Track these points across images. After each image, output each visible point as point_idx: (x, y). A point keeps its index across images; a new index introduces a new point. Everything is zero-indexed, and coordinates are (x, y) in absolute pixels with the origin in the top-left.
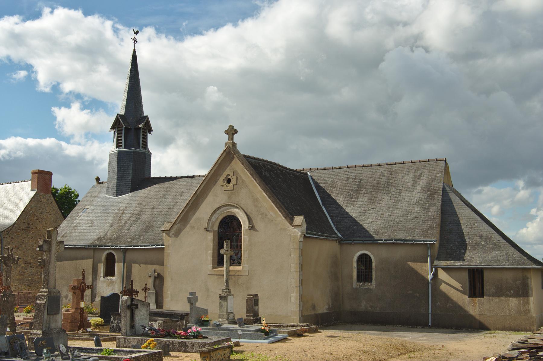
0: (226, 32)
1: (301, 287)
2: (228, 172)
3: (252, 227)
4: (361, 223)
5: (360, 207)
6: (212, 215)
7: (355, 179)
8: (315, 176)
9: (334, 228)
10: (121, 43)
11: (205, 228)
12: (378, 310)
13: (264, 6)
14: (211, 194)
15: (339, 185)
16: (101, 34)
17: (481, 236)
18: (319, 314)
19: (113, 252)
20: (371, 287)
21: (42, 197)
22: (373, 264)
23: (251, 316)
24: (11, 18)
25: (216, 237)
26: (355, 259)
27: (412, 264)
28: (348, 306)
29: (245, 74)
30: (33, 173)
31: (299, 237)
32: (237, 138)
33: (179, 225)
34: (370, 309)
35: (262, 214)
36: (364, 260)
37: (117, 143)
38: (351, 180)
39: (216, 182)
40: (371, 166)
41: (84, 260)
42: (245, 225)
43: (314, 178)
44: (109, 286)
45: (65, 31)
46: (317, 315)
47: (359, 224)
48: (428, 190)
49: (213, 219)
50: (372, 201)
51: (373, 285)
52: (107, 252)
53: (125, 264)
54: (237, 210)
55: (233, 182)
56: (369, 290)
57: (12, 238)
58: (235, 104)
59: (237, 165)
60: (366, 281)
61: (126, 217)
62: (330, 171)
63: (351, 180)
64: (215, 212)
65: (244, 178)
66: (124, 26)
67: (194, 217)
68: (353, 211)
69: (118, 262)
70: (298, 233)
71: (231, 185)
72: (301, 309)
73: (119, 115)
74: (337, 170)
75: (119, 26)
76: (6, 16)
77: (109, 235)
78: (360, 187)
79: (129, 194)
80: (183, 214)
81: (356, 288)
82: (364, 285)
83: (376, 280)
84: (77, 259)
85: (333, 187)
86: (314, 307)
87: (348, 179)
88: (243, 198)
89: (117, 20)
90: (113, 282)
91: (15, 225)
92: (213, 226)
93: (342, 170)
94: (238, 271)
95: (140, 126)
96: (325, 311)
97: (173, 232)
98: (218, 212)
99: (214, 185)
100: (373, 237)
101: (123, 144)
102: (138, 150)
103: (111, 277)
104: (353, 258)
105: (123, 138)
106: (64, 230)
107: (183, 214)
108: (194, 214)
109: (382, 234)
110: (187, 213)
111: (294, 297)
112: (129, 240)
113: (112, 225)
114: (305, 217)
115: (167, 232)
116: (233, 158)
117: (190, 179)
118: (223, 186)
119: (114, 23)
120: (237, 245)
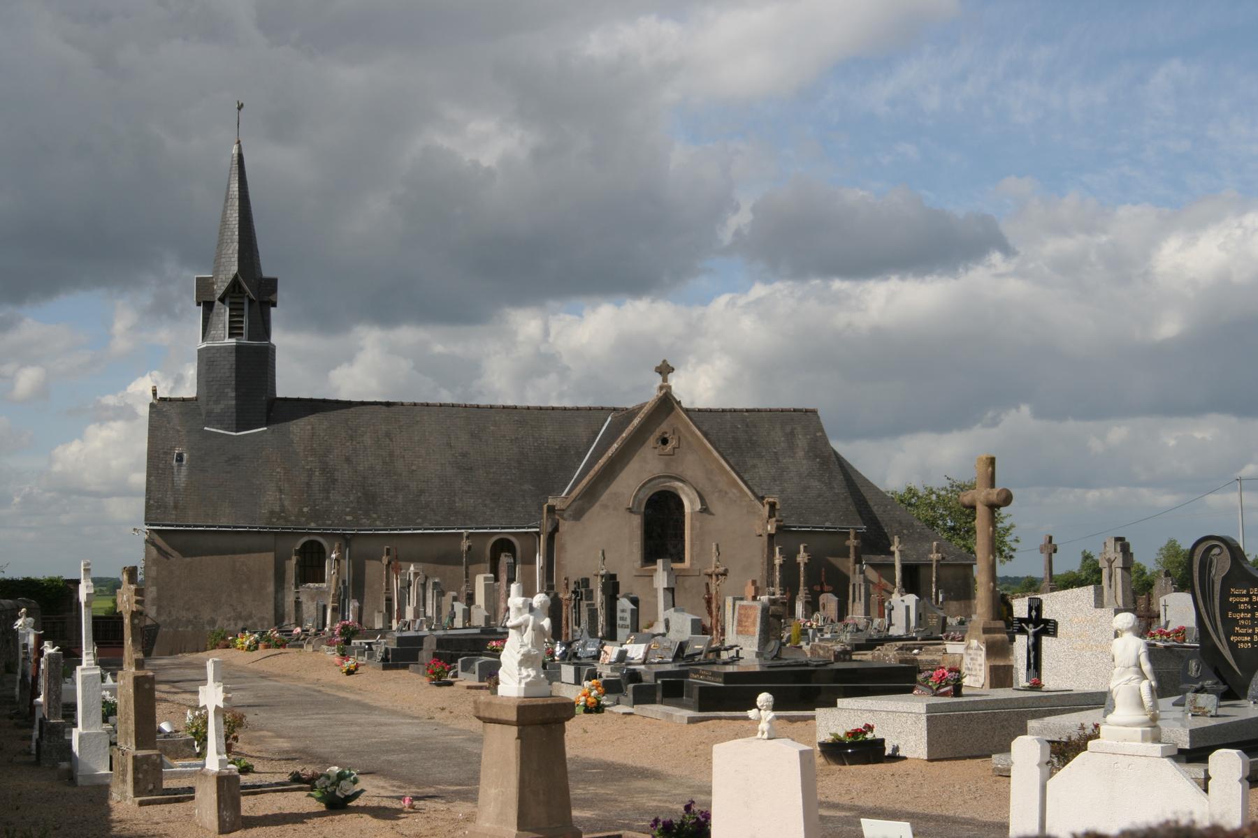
2: (664, 427)
17: (900, 523)
19: (513, 539)
27: (833, 560)
39: (644, 442)
42: (690, 505)
48: (816, 456)
52: (305, 539)
54: (680, 484)
55: (672, 443)
67: (608, 491)
71: (669, 447)
88: (690, 465)
108: (607, 486)
117: (384, 408)
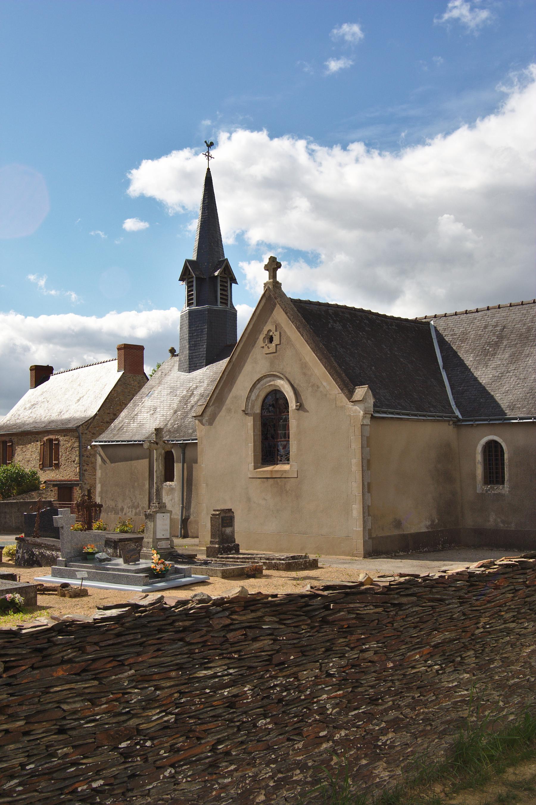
0: (462, 137)
1: (368, 495)
2: (269, 326)
3: (300, 407)
4: (492, 393)
5: (495, 368)
6: (251, 391)
7: (496, 326)
8: (441, 325)
9: (452, 403)
10: (321, 169)
11: (243, 411)
12: (513, 527)
13: (513, 93)
14: (249, 360)
15: (472, 337)
16: (292, 159)
18: (411, 535)
20: (503, 492)
21: (131, 379)
22: (506, 456)
23: (216, 543)
24: (181, 152)
25: (259, 423)
26: (479, 449)
28: (470, 520)
29: (493, 193)
30: (119, 349)
31: (361, 418)
32: (280, 274)
33: (213, 407)
34: (502, 525)
35: (313, 386)
36: (493, 451)
37: (189, 300)
38: (490, 328)
40: (522, 304)
41: (139, 461)
42: (292, 405)
43: (438, 328)
44: (168, 495)
45: (248, 160)
46: (404, 537)
47: (489, 394)
49: (253, 397)
50: (514, 358)
51: (505, 489)
53: (185, 465)
55: (276, 341)
56: (500, 496)
57: (93, 434)
58: (482, 238)
59: (279, 315)
60: (498, 483)
61: (193, 400)
62: (462, 316)
63: (490, 328)
64: (254, 386)
65: (289, 333)
66: (321, 146)
67: (231, 395)
68: (484, 375)
69: (177, 462)
70: (358, 411)
71: (273, 345)
72: (369, 526)
73: (188, 261)
74: (473, 314)
75: (313, 147)
76: (174, 152)
77: (169, 426)
78: (501, 337)
79: (204, 369)
80: (217, 391)
81: (482, 494)
82: (493, 489)
83: (510, 480)
84: (131, 459)
85: (462, 341)
86: (398, 524)
87: (486, 327)
89: (312, 139)
90: (173, 489)
91: (97, 417)
92: (253, 406)
93: (480, 313)
94: (285, 471)
95: (216, 274)
96: (424, 530)
97: (206, 418)
98: (259, 386)
99: (253, 346)
100: (505, 414)
101: (194, 301)
102: (215, 308)
103: (170, 483)
104: (476, 447)
105: (194, 292)
106: (122, 421)
107: (217, 391)
108: (230, 390)
109: (519, 408)
110: (222, 389)
111: (356, 510)
112: (190, 431)
113: (175, 412)
114: (370, 388)
115: (200, 418)
116: (275, 306)
118: (263, 347)
119: (308, 143)
120: (285, 433)
